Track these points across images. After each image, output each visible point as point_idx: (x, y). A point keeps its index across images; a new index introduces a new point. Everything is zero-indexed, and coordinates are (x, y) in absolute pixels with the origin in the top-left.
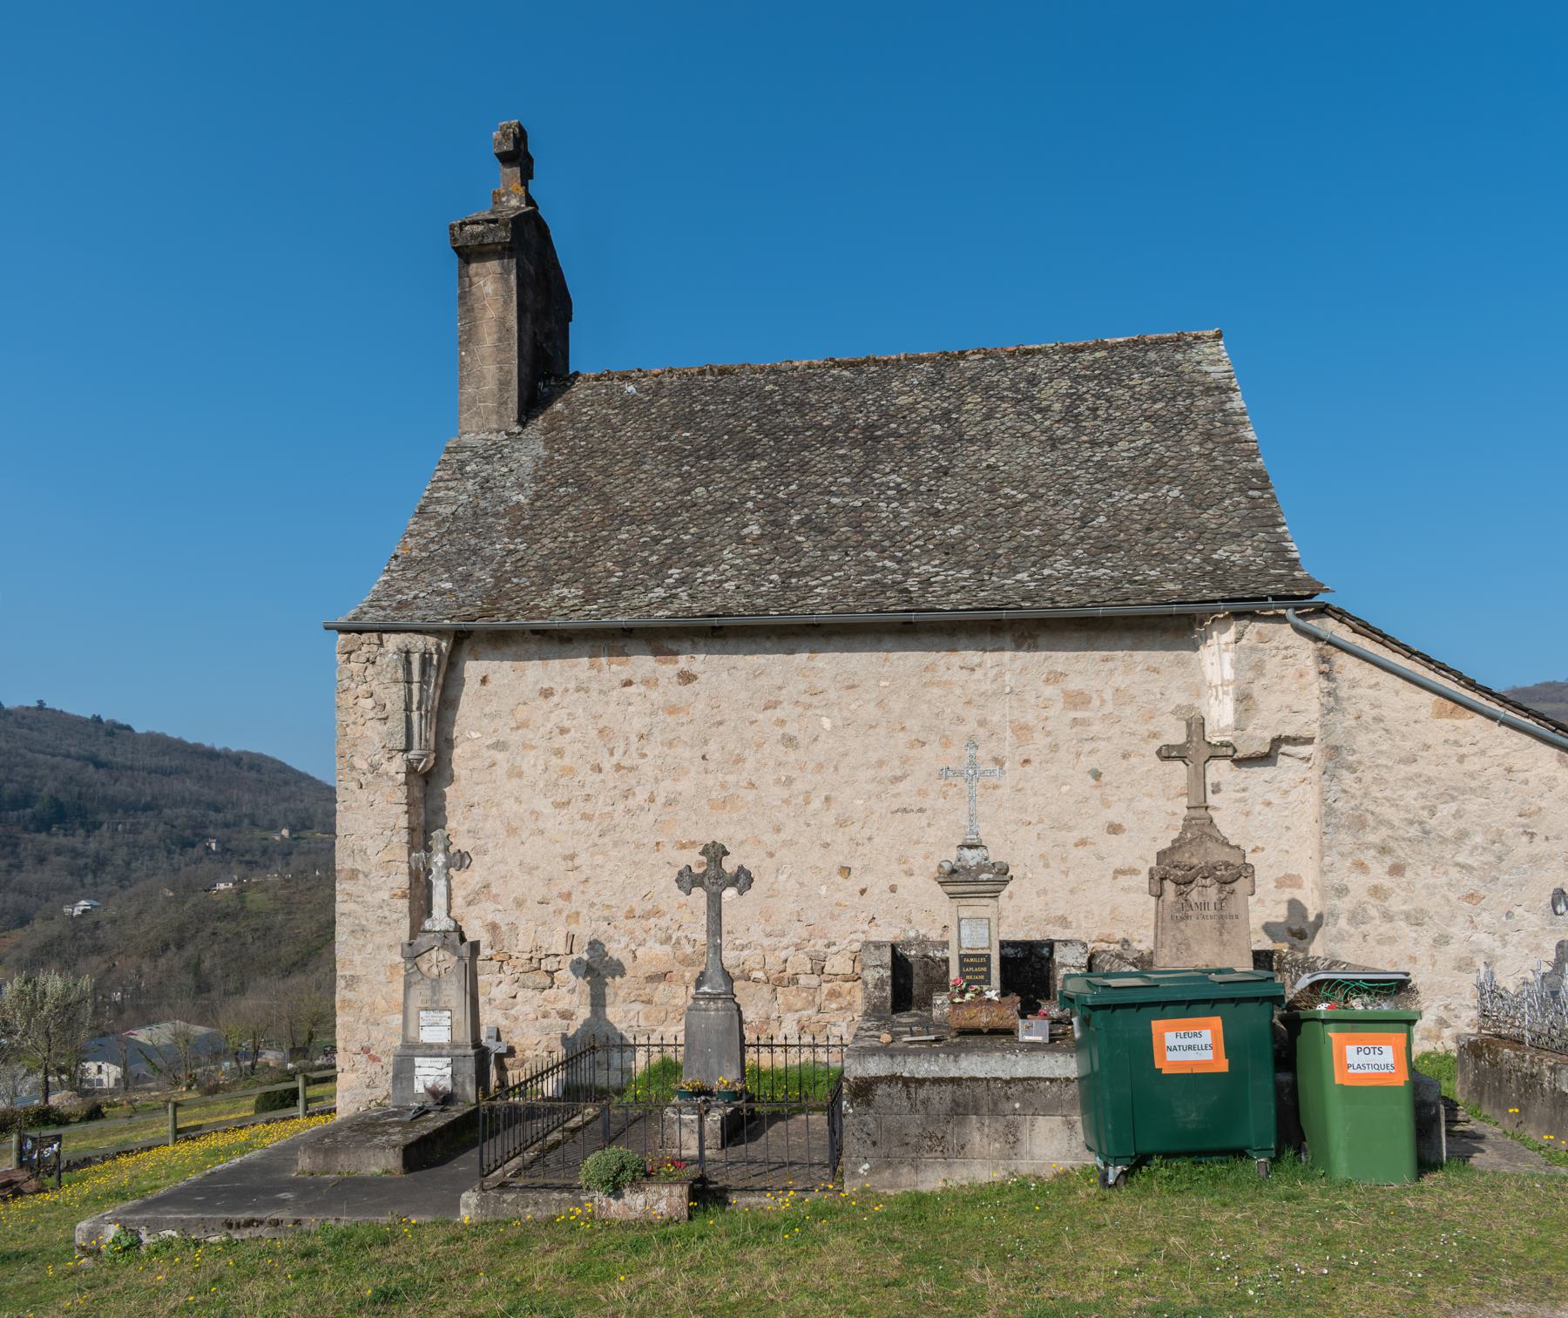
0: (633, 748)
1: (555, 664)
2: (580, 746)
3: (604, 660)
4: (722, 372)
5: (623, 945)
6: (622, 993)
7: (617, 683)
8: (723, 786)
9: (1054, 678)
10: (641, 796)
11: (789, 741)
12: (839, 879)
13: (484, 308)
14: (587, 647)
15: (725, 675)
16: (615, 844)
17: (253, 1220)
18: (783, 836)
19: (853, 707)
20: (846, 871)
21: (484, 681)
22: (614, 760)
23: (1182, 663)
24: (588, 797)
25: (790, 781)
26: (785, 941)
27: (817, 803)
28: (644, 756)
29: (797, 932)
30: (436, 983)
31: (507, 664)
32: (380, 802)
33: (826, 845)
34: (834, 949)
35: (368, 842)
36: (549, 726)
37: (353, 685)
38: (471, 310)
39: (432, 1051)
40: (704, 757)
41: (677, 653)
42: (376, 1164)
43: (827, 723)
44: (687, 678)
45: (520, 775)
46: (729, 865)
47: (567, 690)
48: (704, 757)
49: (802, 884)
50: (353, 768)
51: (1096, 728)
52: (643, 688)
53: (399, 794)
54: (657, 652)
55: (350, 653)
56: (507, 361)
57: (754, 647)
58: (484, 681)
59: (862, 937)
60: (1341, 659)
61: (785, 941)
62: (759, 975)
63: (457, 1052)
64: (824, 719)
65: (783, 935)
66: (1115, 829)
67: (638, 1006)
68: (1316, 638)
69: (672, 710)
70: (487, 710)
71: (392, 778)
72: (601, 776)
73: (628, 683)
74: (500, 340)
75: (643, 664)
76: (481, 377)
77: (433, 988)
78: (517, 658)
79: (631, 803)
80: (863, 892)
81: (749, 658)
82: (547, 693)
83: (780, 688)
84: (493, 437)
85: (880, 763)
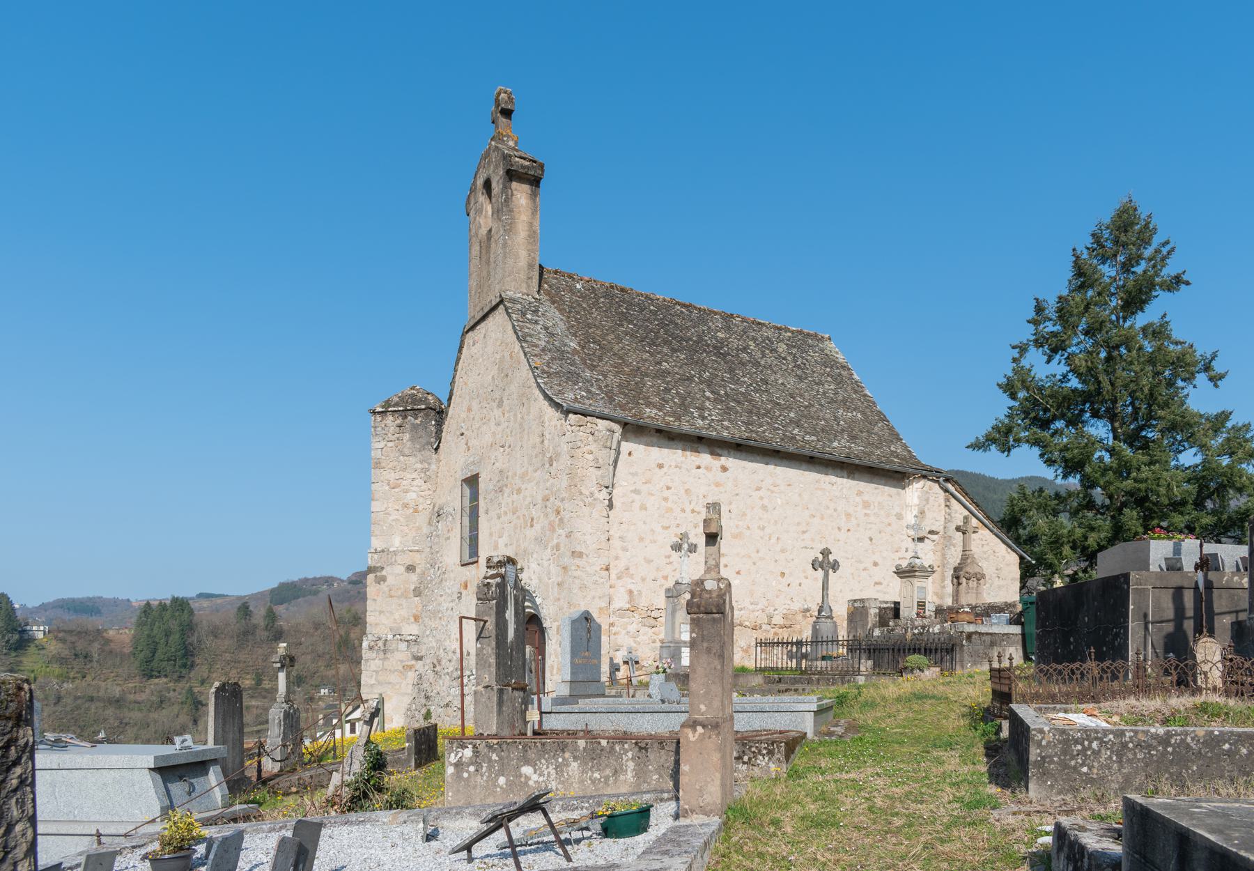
1: (665, 451)
3: (688, 453)
4: (622, 290)
9: (860, 493)
11: (764, 508)
13: (519, 212)
14: (680, 445)
21: (630, 454)
23: (899, 494)
25: (763, 528)
27: (774, 540)
31: (642, 447)
38: (511, 211)
44: (724, 469)
45: (646, 509)
46: (831, 558)
50: (581, 493)
51: (872, 519)
54: (712, 453)
60: (953, 501)
66: (876, 564)
68: (946, 491)
69: (717, 485)
73: (699, 467)
75: (705, 458)
76: (517, 257)
78: (647, 445)
82: (661, 466)
85: (799, 524)
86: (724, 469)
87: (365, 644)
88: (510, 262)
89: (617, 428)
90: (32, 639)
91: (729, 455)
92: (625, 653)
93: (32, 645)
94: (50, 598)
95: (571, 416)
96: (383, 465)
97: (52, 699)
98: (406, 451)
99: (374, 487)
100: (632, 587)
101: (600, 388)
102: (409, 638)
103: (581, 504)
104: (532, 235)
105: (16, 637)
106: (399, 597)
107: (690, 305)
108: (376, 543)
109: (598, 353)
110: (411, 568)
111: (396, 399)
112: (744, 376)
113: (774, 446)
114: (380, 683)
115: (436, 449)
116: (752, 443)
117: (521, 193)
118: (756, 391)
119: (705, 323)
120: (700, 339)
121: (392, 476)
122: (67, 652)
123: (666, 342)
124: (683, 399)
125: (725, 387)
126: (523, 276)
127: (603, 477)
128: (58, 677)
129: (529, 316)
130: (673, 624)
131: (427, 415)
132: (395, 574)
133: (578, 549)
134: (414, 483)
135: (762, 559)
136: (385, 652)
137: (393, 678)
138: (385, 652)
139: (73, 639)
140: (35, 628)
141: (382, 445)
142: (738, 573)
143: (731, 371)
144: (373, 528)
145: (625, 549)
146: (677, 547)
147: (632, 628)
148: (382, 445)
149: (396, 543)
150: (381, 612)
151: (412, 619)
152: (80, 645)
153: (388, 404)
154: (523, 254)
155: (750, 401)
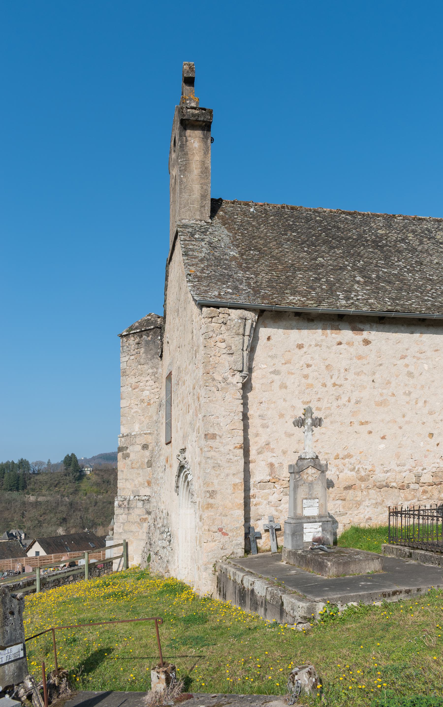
0: (342, 375)
1: (305, 332)
2: (316, 373)
3: (329, 331)
4: (292, 208)
5: (333, 473)
6: (332, 496)
7: (335, 343)
8: (381, 395)
10: (344, 399)
11: (410, 374)
12: (428, 439)
13: (193, 154)
14: (320, 325)
15: (383, 342)
16: (332, 423)
17: (397, 591)
18: (406, 419)
19: (437, 359)
20: (431, 435)
21: (269, 338)
22: (333, 381)
24: (319, 400)
25: (410, 393)
26: (406, 468)
27: (421, 404)
28: (346, 379)
29: (410, 464)
30: (311, 484)
31: (281, 331)
32: (229, 397)
33: (424, 423)
34: (425, 471)
35: (221, 419)
36: (302, 363)
37: (214, 335)
38: (186, 154)
39: (311, 520)
40: (373, 381)
41: (362, 330)
42: (369, 568)
43: (426, 367)
44: (367, 342)
45: (286, 387)
47: (310, 345)
48: (373, 381)
49: (413, 441)
50: (214, 379)
52: (346, 347)
53: (239, 394)
54: (354, 329)
55: (212, 318)
56: (205, 184)
57: (397, 329)
58: (269, 338)
59: (437, 465)
61: (406, 468)
62: (394, 484)
63: (324, 519)
64: (425, 365)
65: (404, 465)
67: (339, 502)
69: (360, 358)
70: (270, 354)
71: (234, 385)
72: (326, 389)
73: (340, 343)
74: (202, 172)
75: (347, 334)
76: (191, 191)
77: (309, 487)
79: (340, 402)
80: (438, 445)
81: (394, 334)
82: (300, 347)
83: (407, 349)
84: (198, 222)
86: (367, 342)
87: (116, 504)
88: (185, 196)
89: (251, 316)
90: (85, 475)
91: (371, 329)
92: (267, 522)
93: (85, 478)
94: (96, 454)
95: (204, 309)
96: (128, 373)
97: (93, 504)
98: (142, 361)
99: (122, 389)
100: (273, 460)
101: (249, 285)
102: (144, 498)
103: (214, 389)
104: (204, 170)
105: (78, 474)
106: (138, 469)
107: (355, 213)
108: (124, 430)
109: (256, 257)
110: (145, 447)
111: (137, 324)
112: (399, 261)
113: (417, 314)
114: (125, 532)
115: (161, 357)
116: (393, 315)
117: (194, 139)
118: (409, 271)
119: (367, 224)
120: (360, 236)
121: (132, 380)
122: (100, 480)
123: (325, 242)
124: (331, 285)
125: (378, 271)
126: (196, 206)
127: (235, 362)
128: (96, 492)
129: (197, 236)
130: (295, 500)
131: (155, 333)
132: (135, 451)
133: (211, 431)
134: (148, 384)
135: (408, 422)
136: (129, 509)
137: (134, 528)
138: (129, 509)
139: (101, 473)
140: (86, 469)
141: (126, 359)
142: (383, 438)
143: (387, 258)
144: (123, 419)
145: (265, 426)
146: (300, 423)
147: (274, 498)
148: (126, 359)
149: (136, 429)
150: (126, 480)
151: (146, 484)
152: (106, 476)
153: (131, 328)
154: (196, 188)
155: (401, 281)
